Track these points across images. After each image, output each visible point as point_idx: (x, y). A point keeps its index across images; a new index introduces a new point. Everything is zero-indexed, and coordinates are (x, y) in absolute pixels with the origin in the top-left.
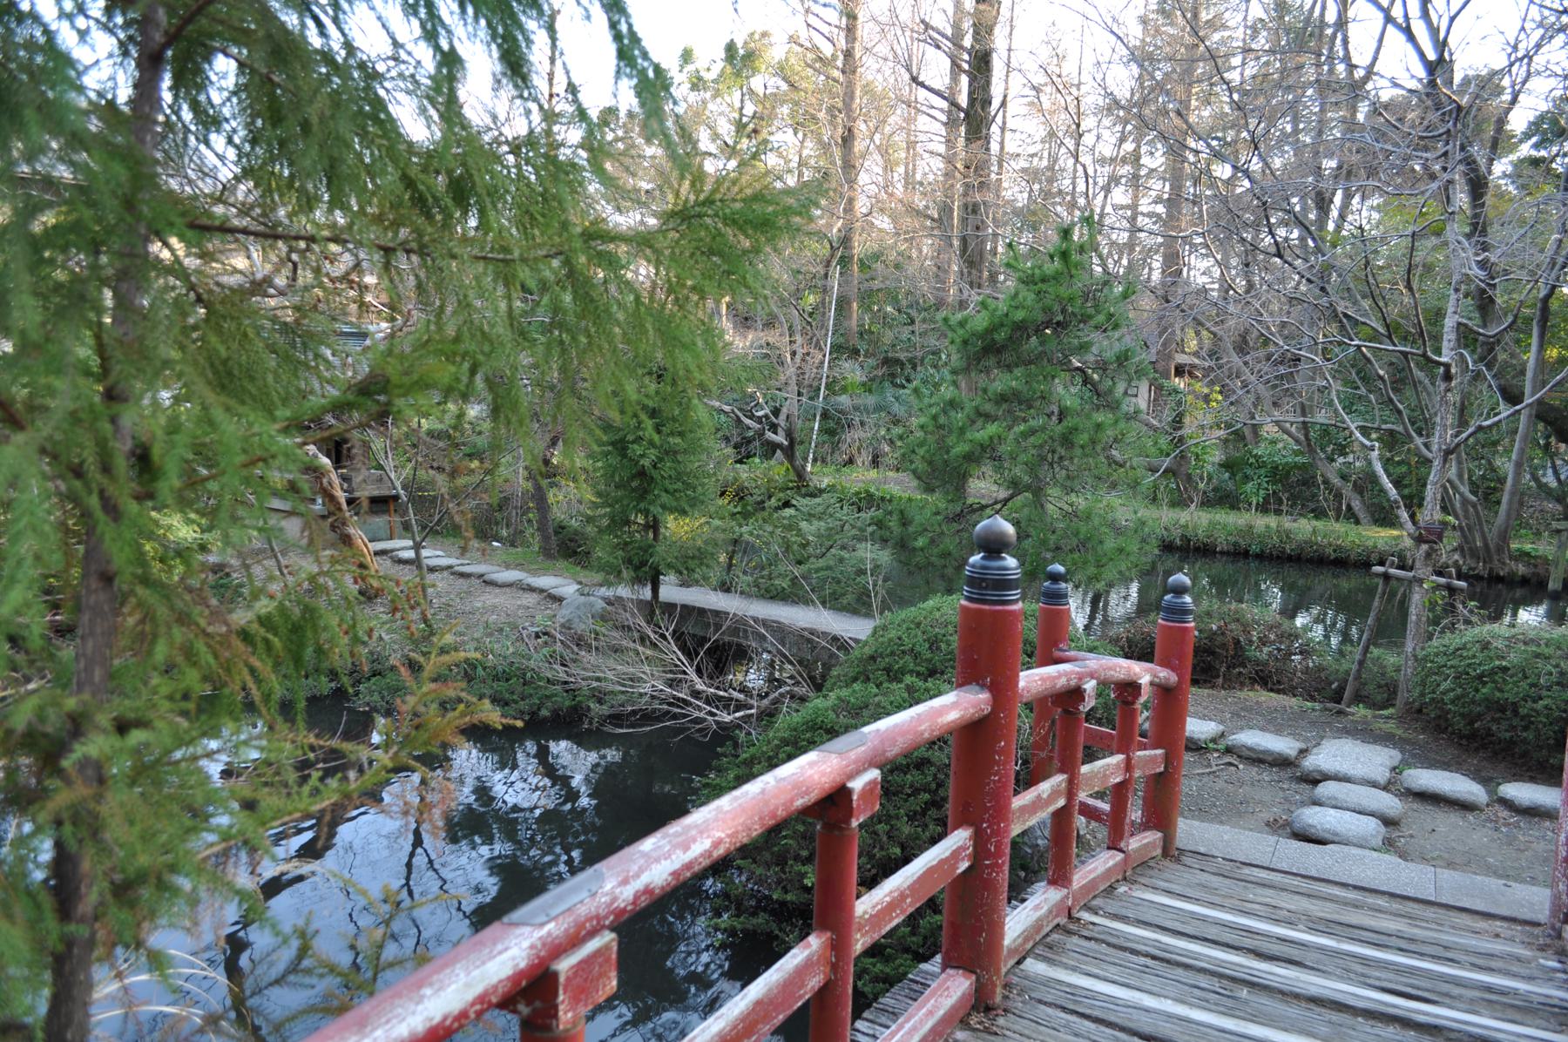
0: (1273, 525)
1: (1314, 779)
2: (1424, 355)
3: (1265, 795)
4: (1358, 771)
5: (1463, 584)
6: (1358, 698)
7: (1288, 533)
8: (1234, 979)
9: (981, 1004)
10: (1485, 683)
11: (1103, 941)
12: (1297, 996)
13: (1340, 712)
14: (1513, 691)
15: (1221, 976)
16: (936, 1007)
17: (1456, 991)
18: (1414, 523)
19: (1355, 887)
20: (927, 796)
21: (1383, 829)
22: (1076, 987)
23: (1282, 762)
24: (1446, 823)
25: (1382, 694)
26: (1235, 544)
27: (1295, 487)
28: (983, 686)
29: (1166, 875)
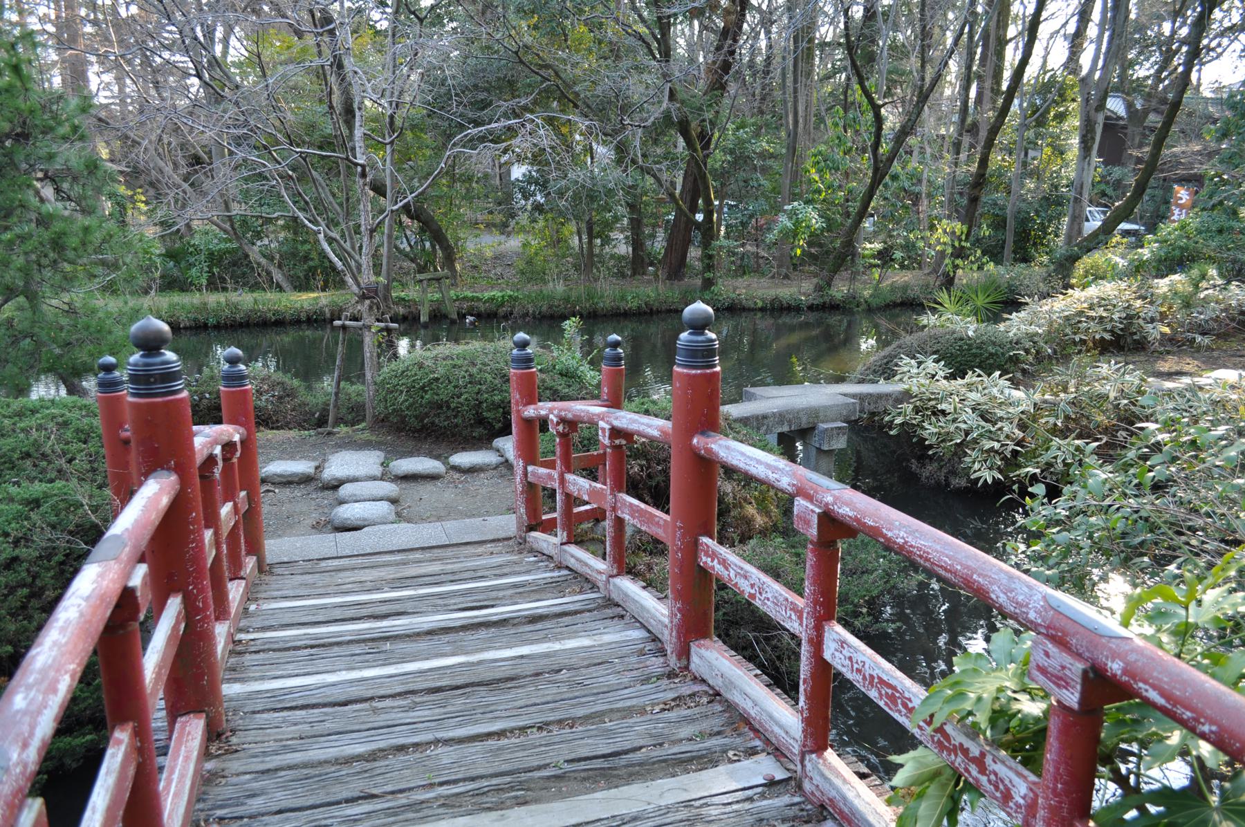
0: (223, 300)
1: (335, 486)
2: (347, 159)
3: (302, 506)
4: (361, 471)
5: (396, 325)
6: (339, 421)
7: (236, 306)
8: (373, 640)
9: (214, 734)
10: (426, 392)
11: (269, 650)
12: (418, 634)
13: (329, 433)
14: (444, 394)
15: (364, 641)
16: (189, 752)
17: (501, 594)
18: (358, 284)
19: (399, 551)
20: (25, 591)
21: (393, 507)
22: (273, 690)
23: (306, 480)
24: (425, 491)
25: (355, 414)
26: (195, 320)
27: (231, 268)
28: (169, 469)
29: (274, 586)
